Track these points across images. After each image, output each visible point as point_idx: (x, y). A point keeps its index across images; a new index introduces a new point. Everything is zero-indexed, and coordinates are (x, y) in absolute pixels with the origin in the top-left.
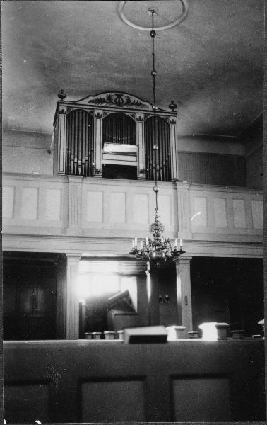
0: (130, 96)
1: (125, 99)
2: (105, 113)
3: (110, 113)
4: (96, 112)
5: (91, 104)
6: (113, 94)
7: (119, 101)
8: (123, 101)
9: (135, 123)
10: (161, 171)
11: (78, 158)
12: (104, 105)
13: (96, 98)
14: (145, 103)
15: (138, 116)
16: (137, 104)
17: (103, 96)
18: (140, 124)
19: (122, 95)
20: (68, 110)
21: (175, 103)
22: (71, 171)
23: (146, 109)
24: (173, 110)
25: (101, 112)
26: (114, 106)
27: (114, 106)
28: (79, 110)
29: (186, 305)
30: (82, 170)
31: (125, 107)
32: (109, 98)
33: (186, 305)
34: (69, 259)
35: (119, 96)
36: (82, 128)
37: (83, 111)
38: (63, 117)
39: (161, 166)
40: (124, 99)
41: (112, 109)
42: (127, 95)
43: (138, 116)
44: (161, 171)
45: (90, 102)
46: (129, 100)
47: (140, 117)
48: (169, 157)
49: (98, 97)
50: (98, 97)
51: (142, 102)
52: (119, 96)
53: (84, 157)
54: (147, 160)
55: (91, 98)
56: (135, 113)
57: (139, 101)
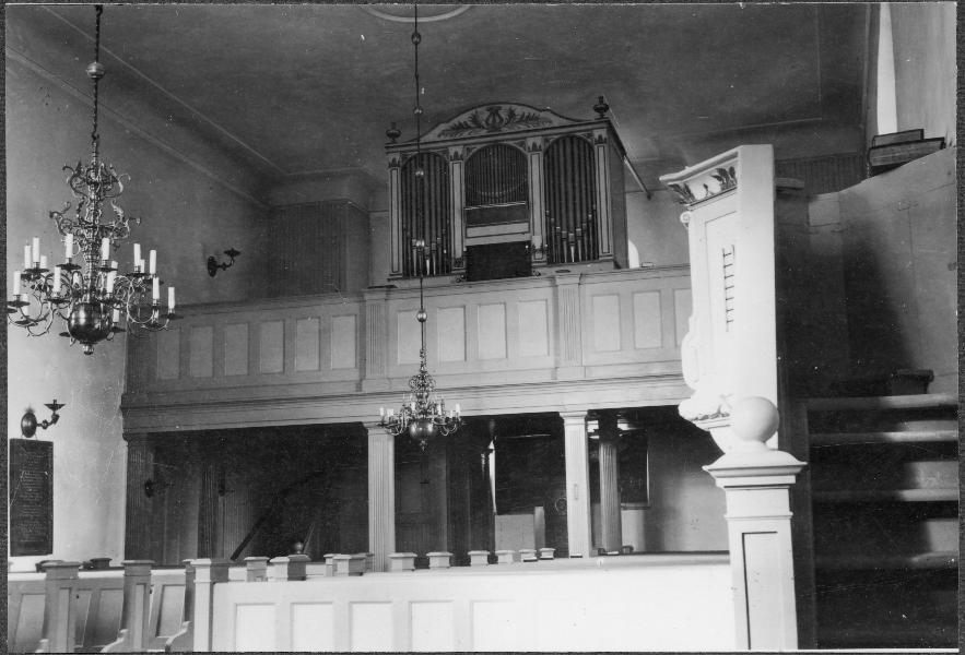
0: (514, 107)
1: (504, 114)
2: (546, 141)
3: (479, 147)
4: (452, 151)
5: (442, 138)
6: (479, 110)
7: (494, 120)
8: (502, 120)
9: (524, 158)
10: (579, 242)
11: (568, 227)
12: (466, 134)
13: (451, 124)
14: (542, 114)
15: (530, 142)
16: (529, 118)
17: (464, 118)
18: (535, 158)
19: (500, 108)
20: (404, 157)
21: (606, 101)
22: (413, 271)
23: (547, 125)
24: (602, 116)
25: (460, 150)
26: (484, 132)
27: (484, 132)
28: (493, 146)
29: (575, 485)
30: (576, 250)
31: (505, 130)
32: (474, 119)
33: (575, 485)
34: (370, 432)
35: (494, 112)
36: (579, 165)
37: (572, 138)
38: (457, 167)
39: (434, 247)
40: (503, 116)
41: (480, 139)
42: (508, 106)
43: (530, 142)
44: (579, 242)
45: (443, 133)
46: (512, 114)
47: (456, 153)
48: (594, 212)
49: (455, 121)
50: (455, 121)
51: (537, 113)
52: (494, 112)
53: (434, 239)
54: (549, 226)
55: (443, 127)
56: (525, 138)
57: (532, 112)
